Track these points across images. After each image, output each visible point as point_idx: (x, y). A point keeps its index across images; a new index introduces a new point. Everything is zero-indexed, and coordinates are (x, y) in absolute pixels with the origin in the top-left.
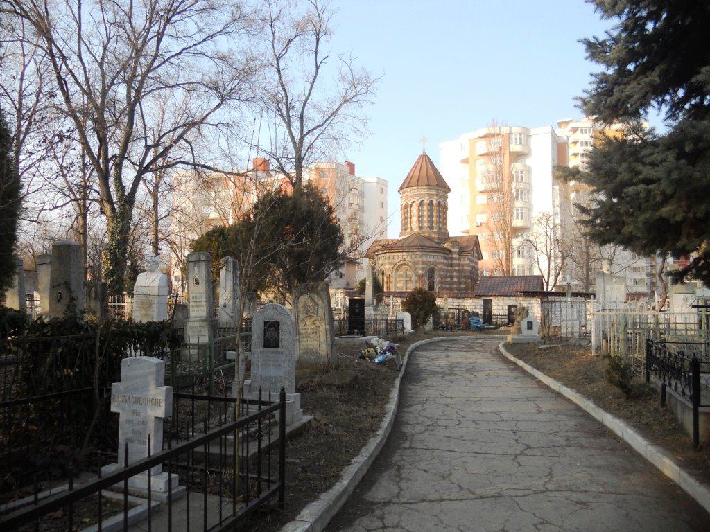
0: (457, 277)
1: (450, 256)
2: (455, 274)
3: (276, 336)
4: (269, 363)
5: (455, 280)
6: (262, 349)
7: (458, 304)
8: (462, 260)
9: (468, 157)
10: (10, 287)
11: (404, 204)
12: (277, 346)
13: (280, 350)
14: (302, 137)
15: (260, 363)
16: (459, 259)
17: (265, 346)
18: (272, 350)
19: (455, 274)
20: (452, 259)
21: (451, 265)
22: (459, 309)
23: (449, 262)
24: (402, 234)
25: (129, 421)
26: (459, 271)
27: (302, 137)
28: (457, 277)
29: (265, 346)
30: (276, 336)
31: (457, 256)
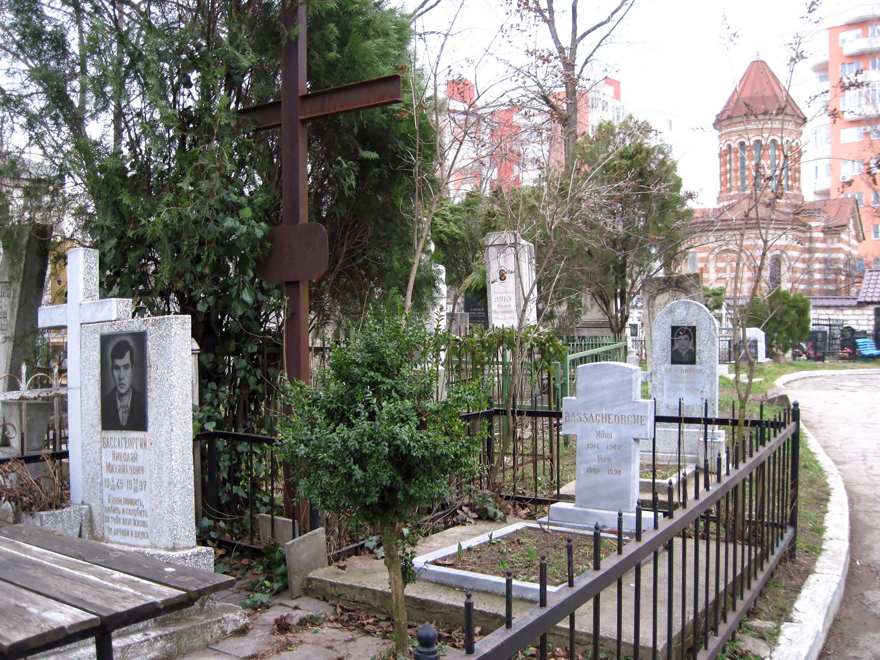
0: (820, 271)
1: (808, 235)
2: (817, 266)
3: (691, 347)
4: (680, 386)
5: (817, 276)
6: (668, 365)
7: (826, 317)
8: (829, 241)
9: (826, 58)
10: (30, 385)
11: (724, 148)
12: (693, 362)
13: (697, 367)
14: (575, 42)
15: (665, 387)
16: (824, 241)
17: (673, 362)
18: (684, 367)
19: (817, 266)
20: (811, 240)
21: (810, 251)
22: (830, 325)
23: (807, 245)
24: (720, 199)
25: (185, 414)
26: (825, 261)
27: (575, 42)
28: (820, 271)
29: (673, 362)
30: (691, 347)
31: (821, 235)
